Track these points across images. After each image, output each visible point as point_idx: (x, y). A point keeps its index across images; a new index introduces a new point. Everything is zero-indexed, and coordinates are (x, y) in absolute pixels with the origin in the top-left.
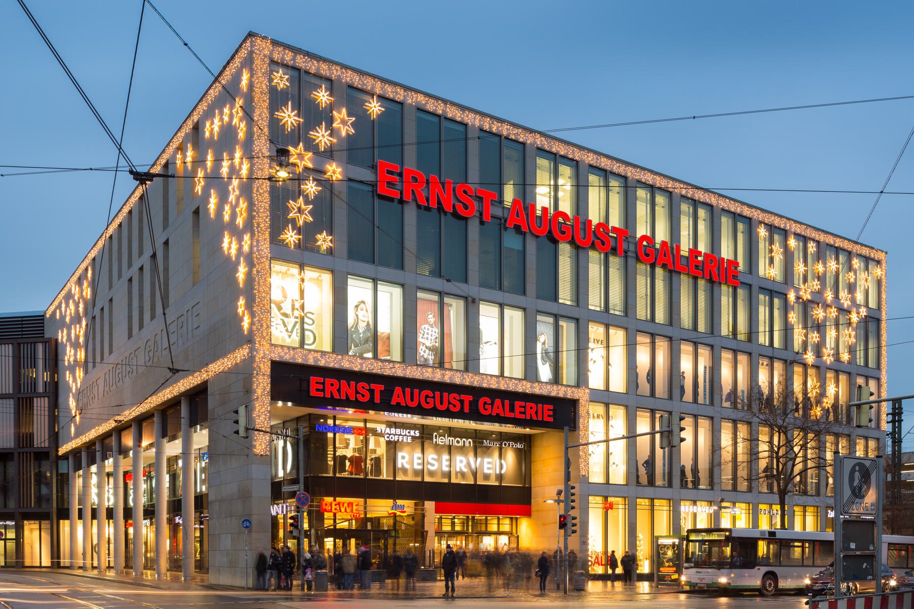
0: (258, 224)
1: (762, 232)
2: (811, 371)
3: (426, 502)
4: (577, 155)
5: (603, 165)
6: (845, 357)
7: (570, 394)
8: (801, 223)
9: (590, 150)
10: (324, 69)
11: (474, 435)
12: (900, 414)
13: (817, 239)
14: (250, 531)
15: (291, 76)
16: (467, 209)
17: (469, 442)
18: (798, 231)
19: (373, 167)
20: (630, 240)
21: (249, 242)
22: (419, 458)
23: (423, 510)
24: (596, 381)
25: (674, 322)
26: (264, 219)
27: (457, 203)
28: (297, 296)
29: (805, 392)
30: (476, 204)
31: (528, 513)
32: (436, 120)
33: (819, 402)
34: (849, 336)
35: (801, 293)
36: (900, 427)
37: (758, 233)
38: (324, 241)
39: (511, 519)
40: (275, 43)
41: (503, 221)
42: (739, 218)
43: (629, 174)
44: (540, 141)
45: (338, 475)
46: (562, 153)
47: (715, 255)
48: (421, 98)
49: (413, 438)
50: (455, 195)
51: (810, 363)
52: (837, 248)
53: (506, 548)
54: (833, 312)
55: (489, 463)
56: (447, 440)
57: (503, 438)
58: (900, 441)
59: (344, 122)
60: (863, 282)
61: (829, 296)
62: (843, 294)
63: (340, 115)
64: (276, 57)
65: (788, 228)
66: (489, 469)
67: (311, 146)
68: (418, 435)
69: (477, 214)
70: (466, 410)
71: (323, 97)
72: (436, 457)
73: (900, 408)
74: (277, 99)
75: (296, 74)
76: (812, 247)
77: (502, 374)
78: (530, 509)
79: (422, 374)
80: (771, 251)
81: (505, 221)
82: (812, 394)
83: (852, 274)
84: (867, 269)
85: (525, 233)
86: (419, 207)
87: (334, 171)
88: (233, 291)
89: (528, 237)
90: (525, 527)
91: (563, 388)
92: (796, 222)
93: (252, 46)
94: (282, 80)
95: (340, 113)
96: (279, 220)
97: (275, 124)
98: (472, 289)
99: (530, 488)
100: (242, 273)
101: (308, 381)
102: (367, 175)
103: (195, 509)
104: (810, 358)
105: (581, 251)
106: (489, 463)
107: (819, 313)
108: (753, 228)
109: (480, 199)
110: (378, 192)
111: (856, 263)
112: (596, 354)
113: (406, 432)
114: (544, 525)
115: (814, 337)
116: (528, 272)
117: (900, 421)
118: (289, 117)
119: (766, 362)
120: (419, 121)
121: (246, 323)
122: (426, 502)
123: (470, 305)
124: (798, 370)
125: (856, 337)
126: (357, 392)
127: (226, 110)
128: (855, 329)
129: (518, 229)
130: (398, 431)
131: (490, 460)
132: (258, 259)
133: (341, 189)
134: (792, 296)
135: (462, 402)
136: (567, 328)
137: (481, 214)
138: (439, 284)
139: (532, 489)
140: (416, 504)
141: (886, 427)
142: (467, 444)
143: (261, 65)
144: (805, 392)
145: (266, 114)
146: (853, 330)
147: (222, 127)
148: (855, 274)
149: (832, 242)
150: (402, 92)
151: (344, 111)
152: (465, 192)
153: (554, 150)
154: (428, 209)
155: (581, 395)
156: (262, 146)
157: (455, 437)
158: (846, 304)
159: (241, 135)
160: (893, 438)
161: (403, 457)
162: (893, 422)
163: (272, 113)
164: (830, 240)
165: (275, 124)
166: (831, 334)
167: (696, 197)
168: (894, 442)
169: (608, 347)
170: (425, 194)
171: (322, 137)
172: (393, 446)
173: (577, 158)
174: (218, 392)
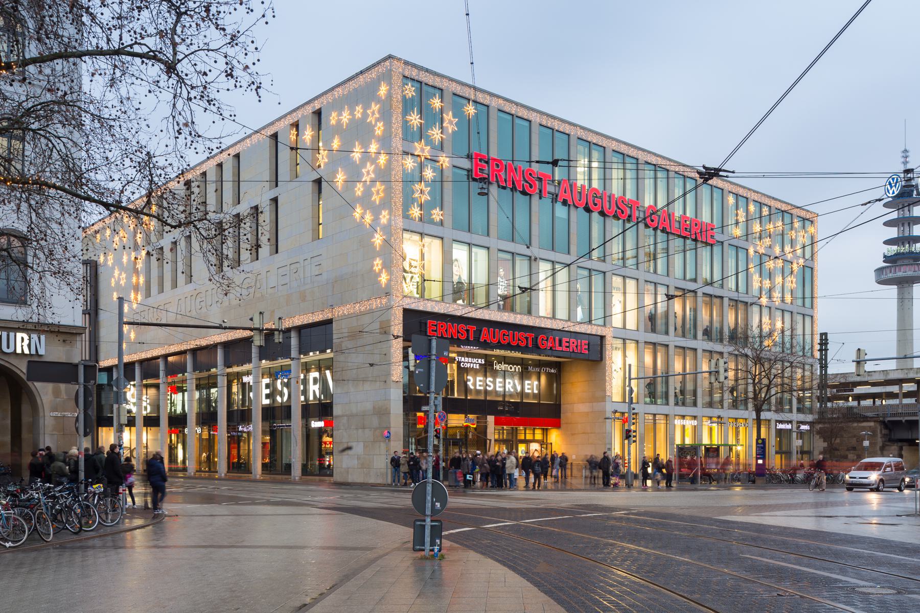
0: (395, 203)
1: (731, 200)
2: (765, 311)
3: (488, 417)
4: (604, 143)
5: (622, 150)
6: (788, 298)
7: (600, 331)
8: (758, 192)
9: (614, 139)
10: (438, 82)
11: (521, 362)
12: (826, 344)
13: (769, 204)
14: (389, 441)
15: (417, 88)
16: (531, 187)
17: (518, 368)
18: (756, 199)
19: (469, 157)
20: (640, 209)
21: (388, 217)
22: (500, 382)
23: (486, 422)
24: (617, 321)
25: (670, 273)
26: (398, 199)
27: (525, 184)
28: (418, 257)
29: (760, 326)
30: (537, 182)
31: (557, 425)
32: (510, 117)
33: (770, 334)
34: (792, 282)
35: (758, 248)
36: (826, 355)
37: (728, 201)
38: (437, 214)
39: (543, 429)
40: (407, 63)
41: (555, 196)
42: (593, 147)
43: (640, 157)
44: (581, 133)
45: (449, 397)
46: (594, 142)
47: (698, 219)
48: (501, 101)
49: (480, 365)
50: (523, 177)
51: (764, 304)
52: (783, 211)
53: (536, 454)
54: (780, 263)
55: (528, 384)
56: (503, 366)
57: (540, 364)
58: (826, 367)
59: (451, 122)
60: (802, 238)
61: (777, 250)
62: (788, 248)
63: (448, 116)
64: (407, 74)
65: (749, 196)
66: (480, 386)
67: (429, 142)
68: (483, 362)
69: (538, 191)
70: (530, 346)
71: (436, 103)
72: (492, 380)
73: (826, 339)
74: (408, 106)
75: (418, 85)
76: (765, 211)
77: (624, 327)
78: (560, 421)
79: (502, 317)
80: (737, 215)
81: (557, 196)
82: (766, 328)
83: (793, 232)
84: (804, 227)
85: (569, 205)
86: (499, 186)
87: (445, 161)
88: (371, 253)
89: (572, 208)
90: (554, 436)
91: (596, 327)
92: (754, 191)
93: (391, 65)
94: (410, 91)
95: (448, 115)
96: (408, 201)
97: (406, 125)
98: (535, 251)
99: (560, 405)
100: (378, 240)
101: (426, 323)
102: (466, 164)
103: (263, 419)
104: (764, 301)
105: (607, 219)
106: (528, 384)
107: (770, 264)
108: (725, 196)
109: (540, 180)
110: (474, 176)
111: (797, 225)
112: (617, 299)
113: (475, 360)
114: (573, 434)
115: (767, 284)
116: (572, 236)
117: (826, 350)
118: (415, 119)
119: (651, 287)
120: (499, 118)
121: (384, 278)
122: (488, 417)
123: (533, 263)
124: (755, 309)
125: (796, 283)
126: (458, 332)
127: (359, 109)
128: (796, 277)
129: (565, 203)
130: (470, 360)
131: (529, 382)
132: (395, 230)
133: (448, 174)
134: (751, 251)
135: (467, 331)
136: (597, 280)
137: (540, 191)
138: (466, 237)
139: (563, 407)
140: (478, 418)
141: (817, 355)
142: (517, 370)
143: (397, 80)
144: (760, 326)
145: (400, 119)
146: (794, 277)
147: (352, 121)
148: (796, 232)
149: (780, 207)
150: (488, 97)
151: (451, 113)
152: (530, 174)
153: (589, 139)
154: (504, 188)
155: (607, 332)
156: (398, 144)
157: (509, 364)
158: (789, 256)
159: (378, 132)
160: (821, 363)
161: (509, 383)
162: (821, 350)
163: (403, 118)
164: (779, 205)
165: (406, 125)
166: (779, 279)
167: (686, 174)
168: (821, 367)
169: (625, 293)
170: (504, 177)
171: (435, 134)
172: (462, 371)
173: (604, 145)
174: (346, 330)
